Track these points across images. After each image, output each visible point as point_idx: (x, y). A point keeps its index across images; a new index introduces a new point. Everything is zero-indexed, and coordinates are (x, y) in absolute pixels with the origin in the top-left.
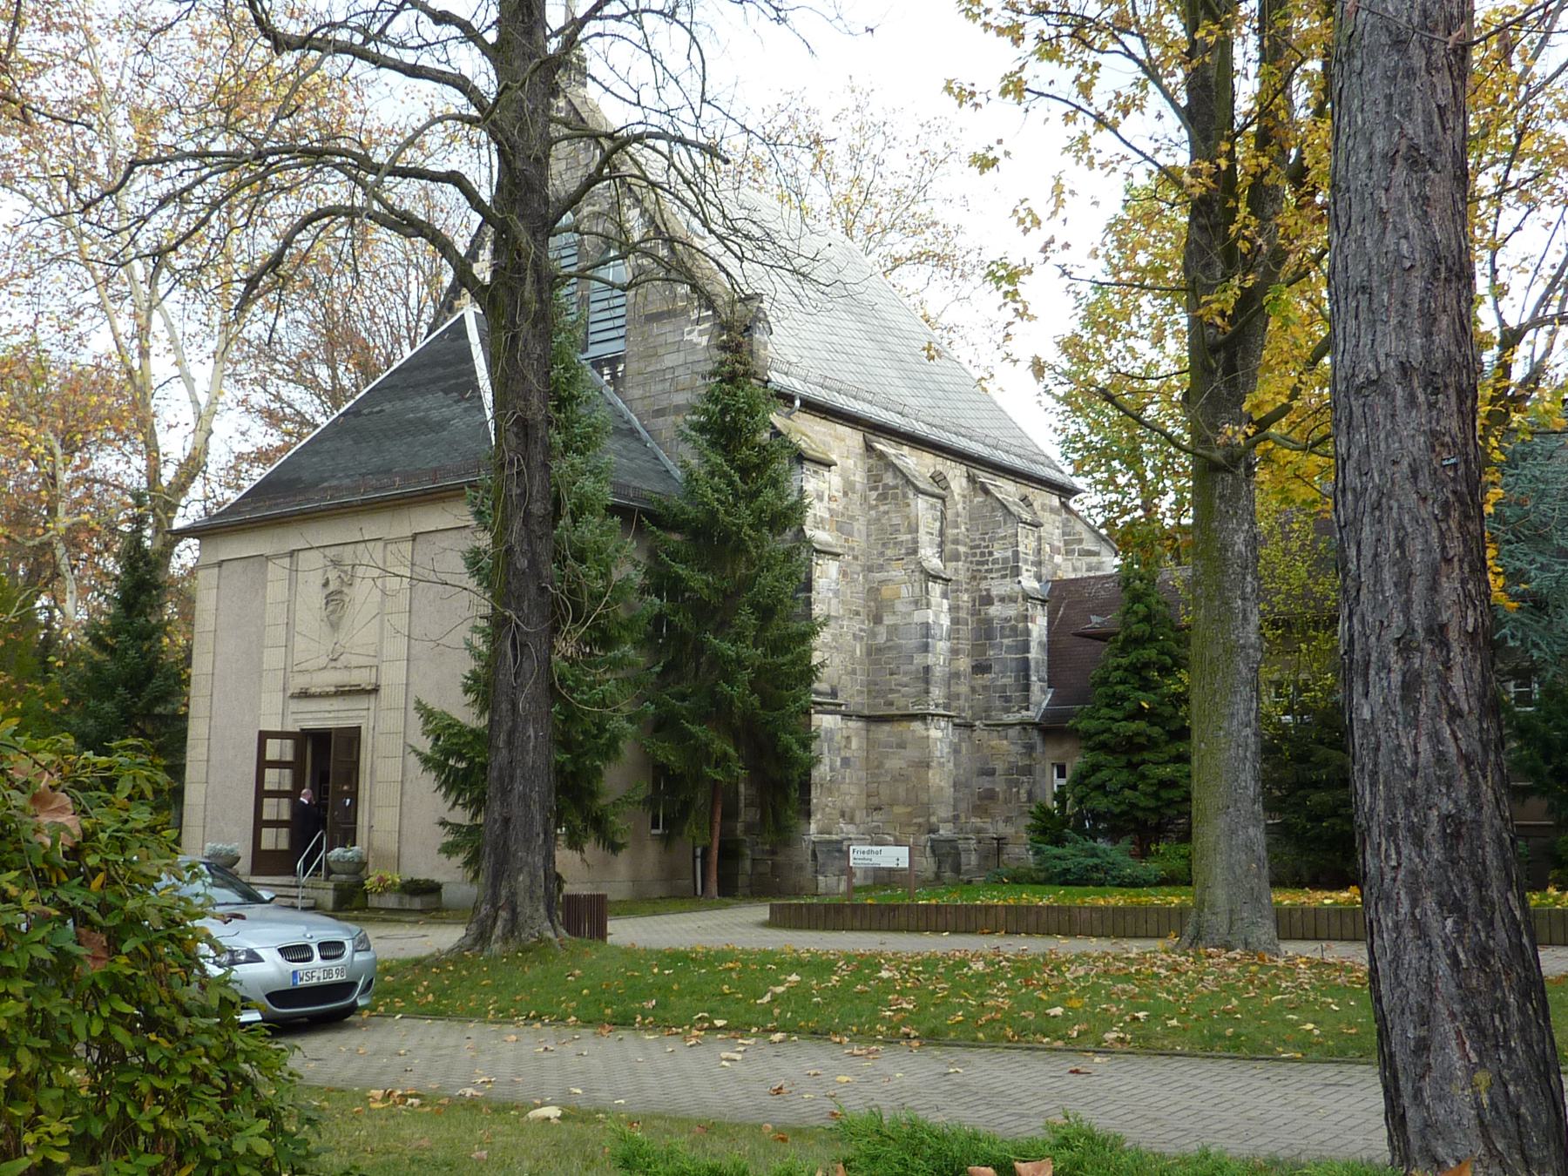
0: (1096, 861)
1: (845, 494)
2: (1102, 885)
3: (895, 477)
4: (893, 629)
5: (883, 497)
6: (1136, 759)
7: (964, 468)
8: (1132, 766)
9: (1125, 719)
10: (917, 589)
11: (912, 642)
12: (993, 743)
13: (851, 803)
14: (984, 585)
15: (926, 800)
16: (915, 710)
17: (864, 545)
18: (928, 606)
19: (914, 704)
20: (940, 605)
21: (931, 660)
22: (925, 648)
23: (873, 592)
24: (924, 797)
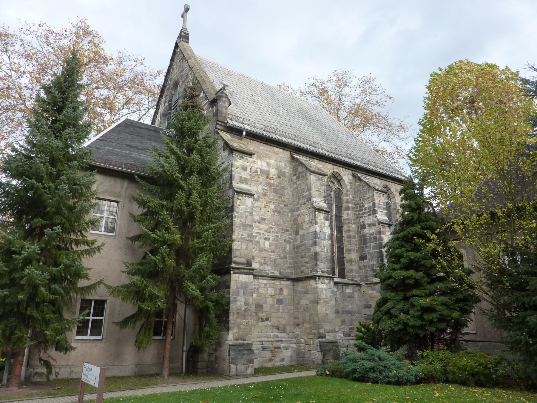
0: (372, 364)
1: (279, 177)
2: (377, 382)
3: (302, 168)
4: (303, 235)
5: (298, 178)
6: (409, 294)
7: (350, 172)
8: (406, 299)
9: (401, 269)
10: (311, 216)
11: (309, 242)
12: (369, 292)
13: (283, 322)
14: (361, 220)
15: (317, 321)
16: (311, 274)
17: (291, 200)
18: (316, 223)
19: (311, 271)
20: (324, 223)
21: (318, 249)
22: (315, 244)
23: (295, 220)
24: (316, 319)
